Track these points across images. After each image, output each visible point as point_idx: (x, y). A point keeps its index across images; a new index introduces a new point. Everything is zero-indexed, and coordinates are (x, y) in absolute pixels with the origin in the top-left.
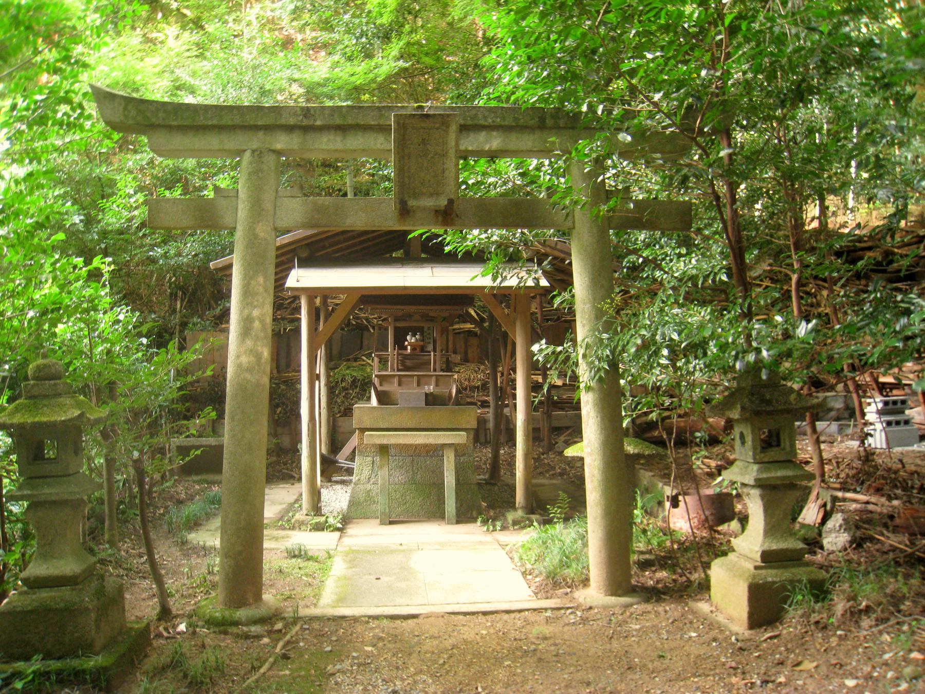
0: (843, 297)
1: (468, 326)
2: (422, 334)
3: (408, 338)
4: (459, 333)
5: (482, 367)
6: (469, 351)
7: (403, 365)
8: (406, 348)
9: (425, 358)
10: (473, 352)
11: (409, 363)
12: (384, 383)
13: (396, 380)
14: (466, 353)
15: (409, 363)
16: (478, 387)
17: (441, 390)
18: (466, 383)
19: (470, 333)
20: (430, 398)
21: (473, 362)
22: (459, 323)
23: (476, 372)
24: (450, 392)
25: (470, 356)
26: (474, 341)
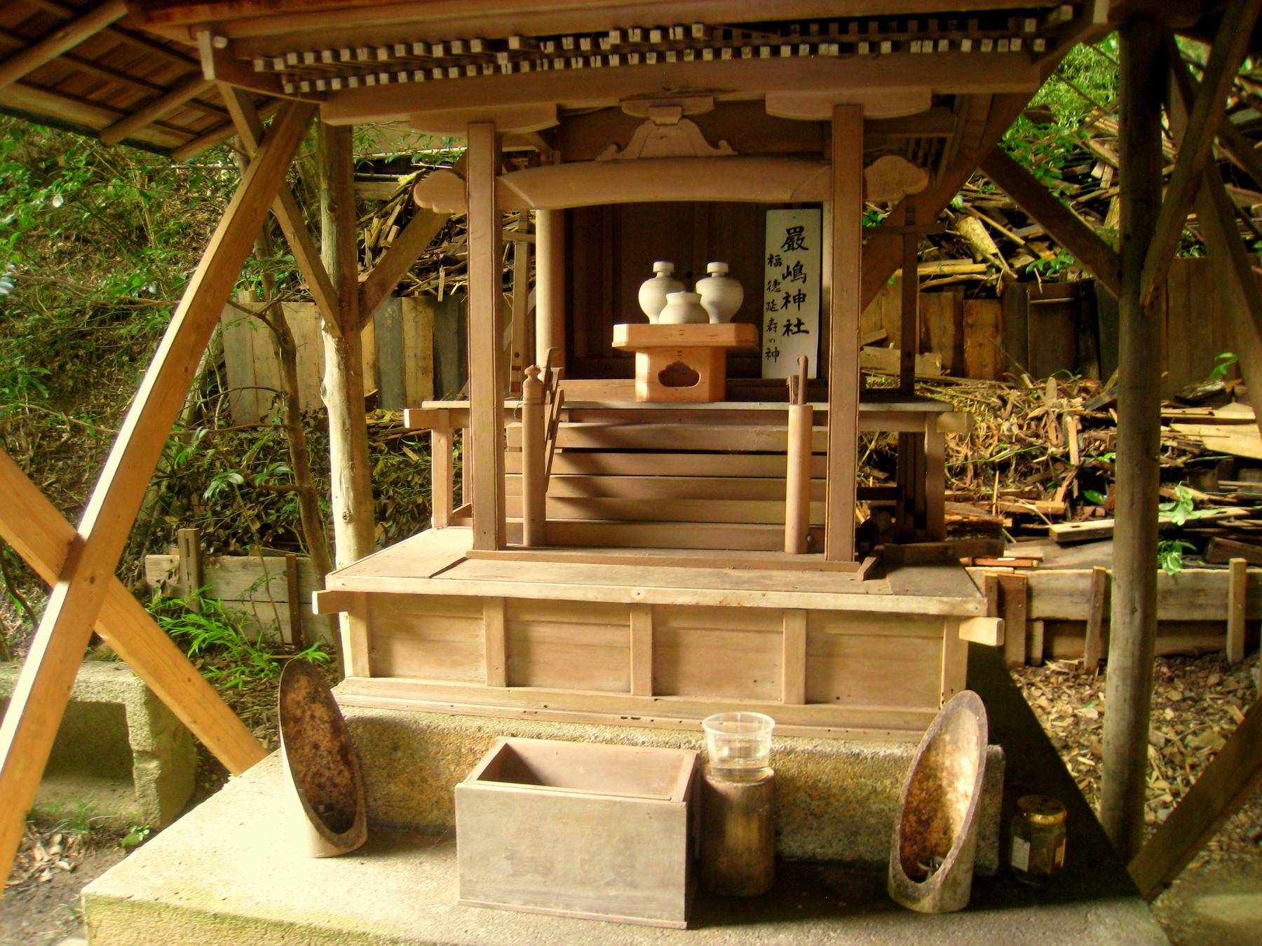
0: (215, 447)
1: (965, 267)
2: (748, 273)
3: (648, 294)
4: (939, 289)
5: (1014, 396)
6: (968, 344)
7: (590, 492)
8: (621, 366)
9: (752, 436)
10: (982, 346)
11: (629, 479)
12: (403, 653)
13: (484, 635)
14: (959, 349)
15: (629, 479)
16: (1003, 467)
17: (855, 744)
18: (964, 450)
19: (971, 287)
20: (742, 835)
21: (981, 377)
22: (936, 259)
23: (995, 411)
24: (927, 772)
25: (971, 354)
26: (985, 313)
